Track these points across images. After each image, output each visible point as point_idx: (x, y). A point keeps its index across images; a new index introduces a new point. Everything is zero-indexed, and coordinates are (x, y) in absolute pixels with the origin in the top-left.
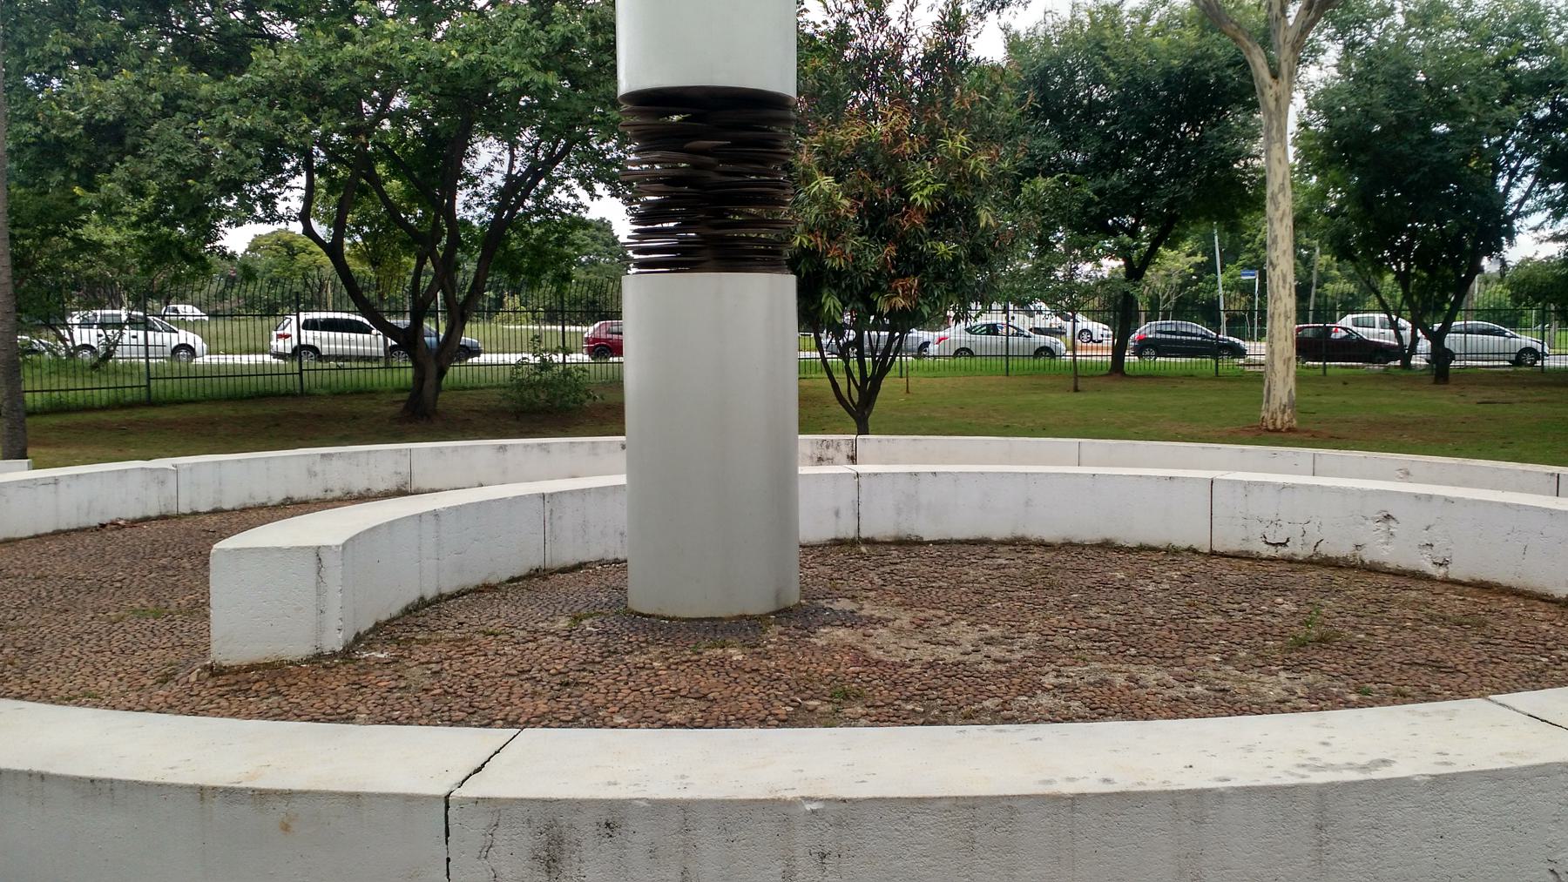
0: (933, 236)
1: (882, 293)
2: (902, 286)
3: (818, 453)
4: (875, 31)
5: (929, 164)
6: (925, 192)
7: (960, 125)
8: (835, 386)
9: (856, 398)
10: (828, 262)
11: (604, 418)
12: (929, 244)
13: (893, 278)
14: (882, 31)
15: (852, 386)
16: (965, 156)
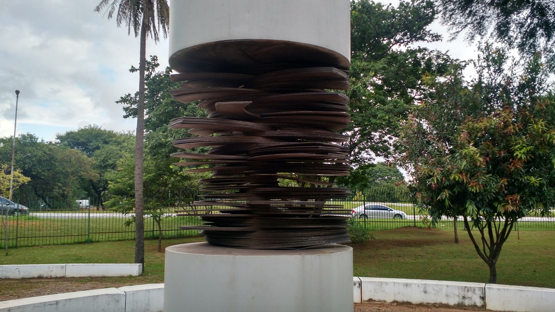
0: (528, 173)
1: (500, 203)
2: (511, 199)
3: (462, 294)
4: (496, 76)
5: (524, 137)
6: (522, 151)
7: (541, 117)
8: (477, 247)
9: (488, 254)
10: (470, 189)
11: (379, 246)
12: (526, 178)
13: (506, 195)
14: (499, 75)
15: (486, 247)
16: (544, 132)
